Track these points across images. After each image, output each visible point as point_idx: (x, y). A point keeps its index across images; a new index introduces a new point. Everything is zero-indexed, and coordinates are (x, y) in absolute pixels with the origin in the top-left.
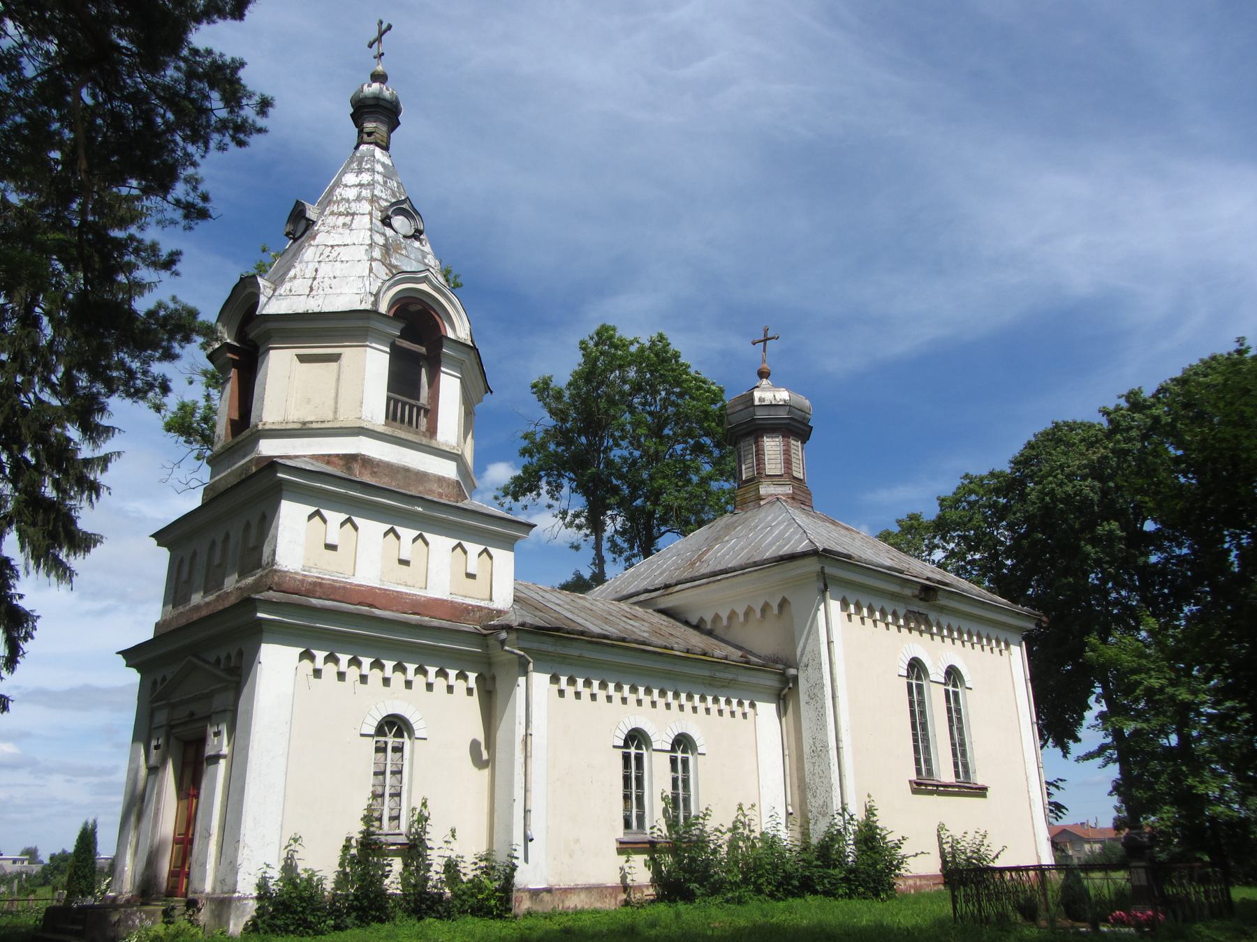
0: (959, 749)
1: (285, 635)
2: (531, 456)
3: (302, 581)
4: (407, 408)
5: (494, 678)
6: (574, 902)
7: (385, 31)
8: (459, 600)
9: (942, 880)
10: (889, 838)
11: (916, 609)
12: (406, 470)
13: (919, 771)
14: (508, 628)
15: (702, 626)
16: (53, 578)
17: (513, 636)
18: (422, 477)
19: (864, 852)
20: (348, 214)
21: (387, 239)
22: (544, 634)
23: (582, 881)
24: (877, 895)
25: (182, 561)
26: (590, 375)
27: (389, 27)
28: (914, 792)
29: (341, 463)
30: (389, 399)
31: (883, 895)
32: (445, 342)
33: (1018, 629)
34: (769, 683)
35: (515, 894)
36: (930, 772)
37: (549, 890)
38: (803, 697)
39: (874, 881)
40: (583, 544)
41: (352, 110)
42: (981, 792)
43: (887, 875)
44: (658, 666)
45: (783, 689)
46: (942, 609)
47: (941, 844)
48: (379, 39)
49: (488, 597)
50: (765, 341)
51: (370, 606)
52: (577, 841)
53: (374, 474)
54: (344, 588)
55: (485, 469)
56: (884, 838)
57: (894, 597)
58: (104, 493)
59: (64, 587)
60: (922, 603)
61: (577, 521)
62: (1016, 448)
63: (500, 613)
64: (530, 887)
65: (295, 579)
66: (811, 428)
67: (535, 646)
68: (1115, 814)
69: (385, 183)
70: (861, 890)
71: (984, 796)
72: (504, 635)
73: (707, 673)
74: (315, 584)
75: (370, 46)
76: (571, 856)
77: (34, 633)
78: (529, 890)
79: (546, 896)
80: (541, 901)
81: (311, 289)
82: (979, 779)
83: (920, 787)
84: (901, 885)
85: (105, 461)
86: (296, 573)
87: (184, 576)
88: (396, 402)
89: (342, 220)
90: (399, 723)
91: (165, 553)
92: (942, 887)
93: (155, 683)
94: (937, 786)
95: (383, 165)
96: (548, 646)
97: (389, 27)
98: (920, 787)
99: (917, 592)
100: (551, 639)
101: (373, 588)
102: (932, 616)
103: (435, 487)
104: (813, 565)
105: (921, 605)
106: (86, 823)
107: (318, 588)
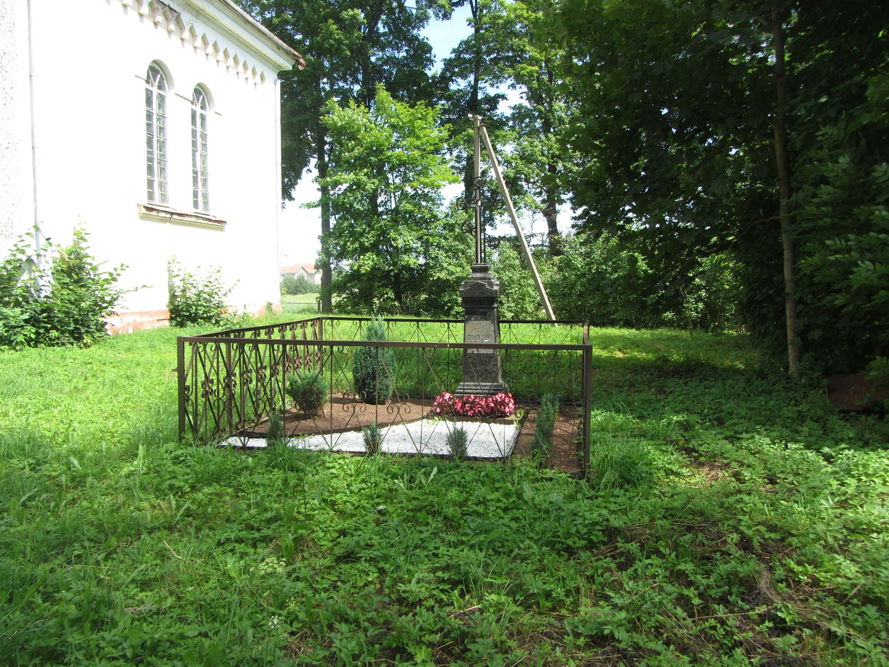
0: (199, 177)
9: (167, 315)
13: (151, 196)
19: (65, 285)
24: (79, 339)
28: (143, 217)
31: (87, 339)
33: (275, 65)
36: (164, 197)
39: (76, 321)
42: (221, 223)
43: (368, 210)
47: (171, 276)
55: (616, 529)
56: (94, 269)
68: (318, 257)
70: (54, 334)
71: (222, 229)
92: (167, 323)
94: (172, 214)
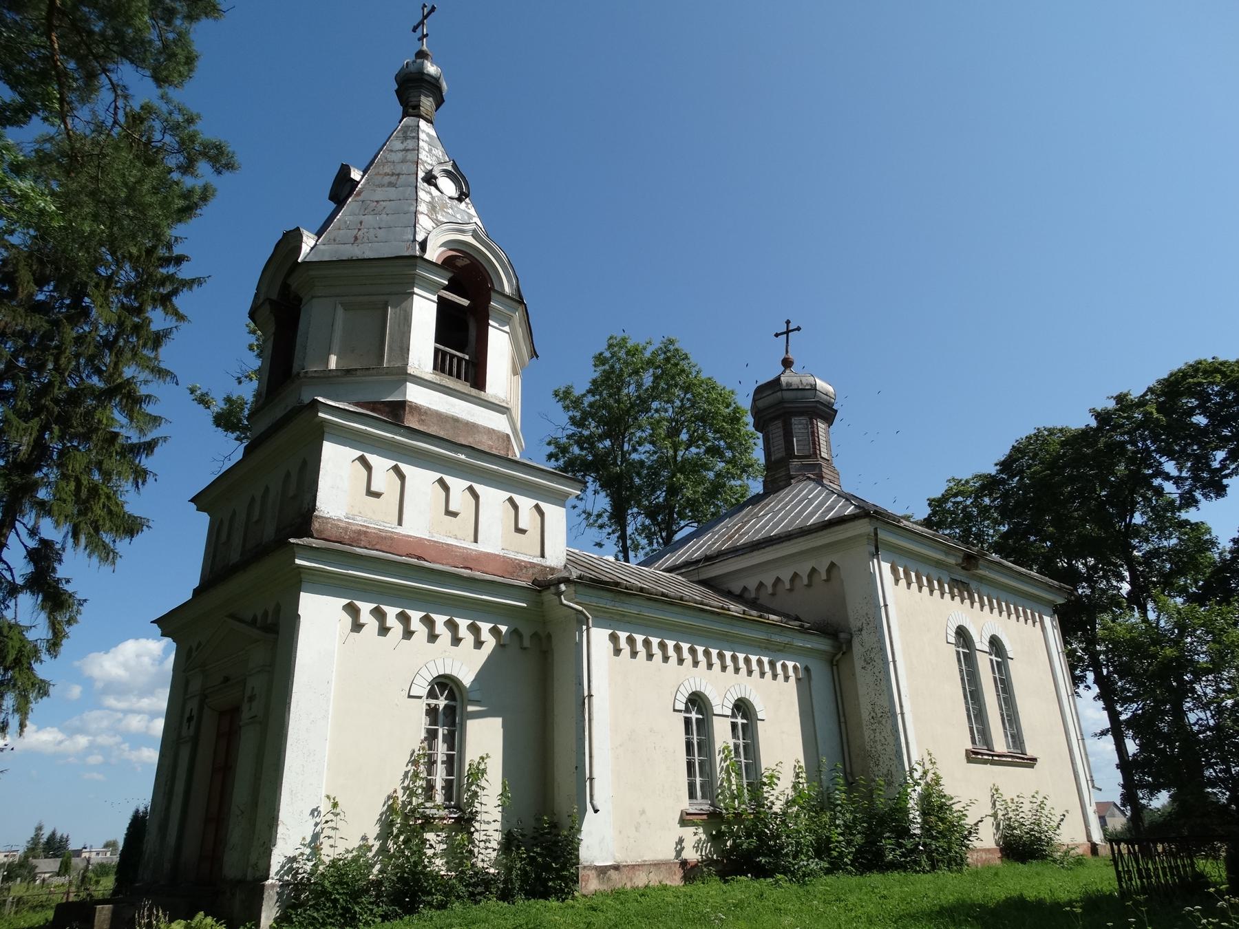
1: (328, 585)
2: (557, 460)
3: (346, 529)
4: (455, 361)
5: (549, 637)
6: (641, 880)
7: (429, 13)
8: (512, 555)
10: (955, 807)
11: (958, 578)
12: (456, 420)
14: (567, 581)
15: (746, 595)
16: (95, 559)
17: (572, 588)
18: (472, 427)
20: (393, 174)
21: (433, 198)
22: (603, 589)
23: (649, 856)
25: (222, 522)
26: (609, 381)
27: (433, 9)
28: (969, 760)
29: (387, 409)
30: (437, 351)
32: (493, 295)
34: (822, 647)
35: (581, 873)
37: (616, 868)
38: (858, 664)
40: (605, 542)
41: (396, 87)
44: (716, 627)
45: (835, 655)
46: (981, 579)
48: (422, 23)
49: (539, 553)
50: (787, 332)
51: (419, 558)
52: (643, 812)
53: (422, 421)
54: (392, 539)
57: (939, 564)
58: (150, 479)
59: (106, 568)
60: (964, 572)
61: (600, 521)
62: (1003, 452)
63: (552, 570)
64: (597, 864)
65: (338, 527)
66: (836, 411)
67: (594, 601)
69: (430, 151)
72: (563, 587)
73: (762, 636)
74: (359, 533)
75: (414, 30)
76: (637, 829)
77: (79, 617)
78: (596, 868)
79: (612, 872)
80: (609, 879)
81: (356, 238)
82: (1030, 752)
83: (972, 757)
84: (971, 858)
85: (149, 447)
86: (339, 520)
87: (224, 537)
88: (444, 354)
89: (387, 179)
90: (451, 684)
91: (205, 518)
93: (190, 650)
95: (428, 135)
96: (605, 601)
97: (433, 9)
98: (972, 757)
99: (960, 561)
100: (609, 595)
101: (421, 539)
102: (973, 585)
103: (485, 438)
104: (864, 527)
105: (963, 577)
106: (137, 811)
107: (360, 536)
